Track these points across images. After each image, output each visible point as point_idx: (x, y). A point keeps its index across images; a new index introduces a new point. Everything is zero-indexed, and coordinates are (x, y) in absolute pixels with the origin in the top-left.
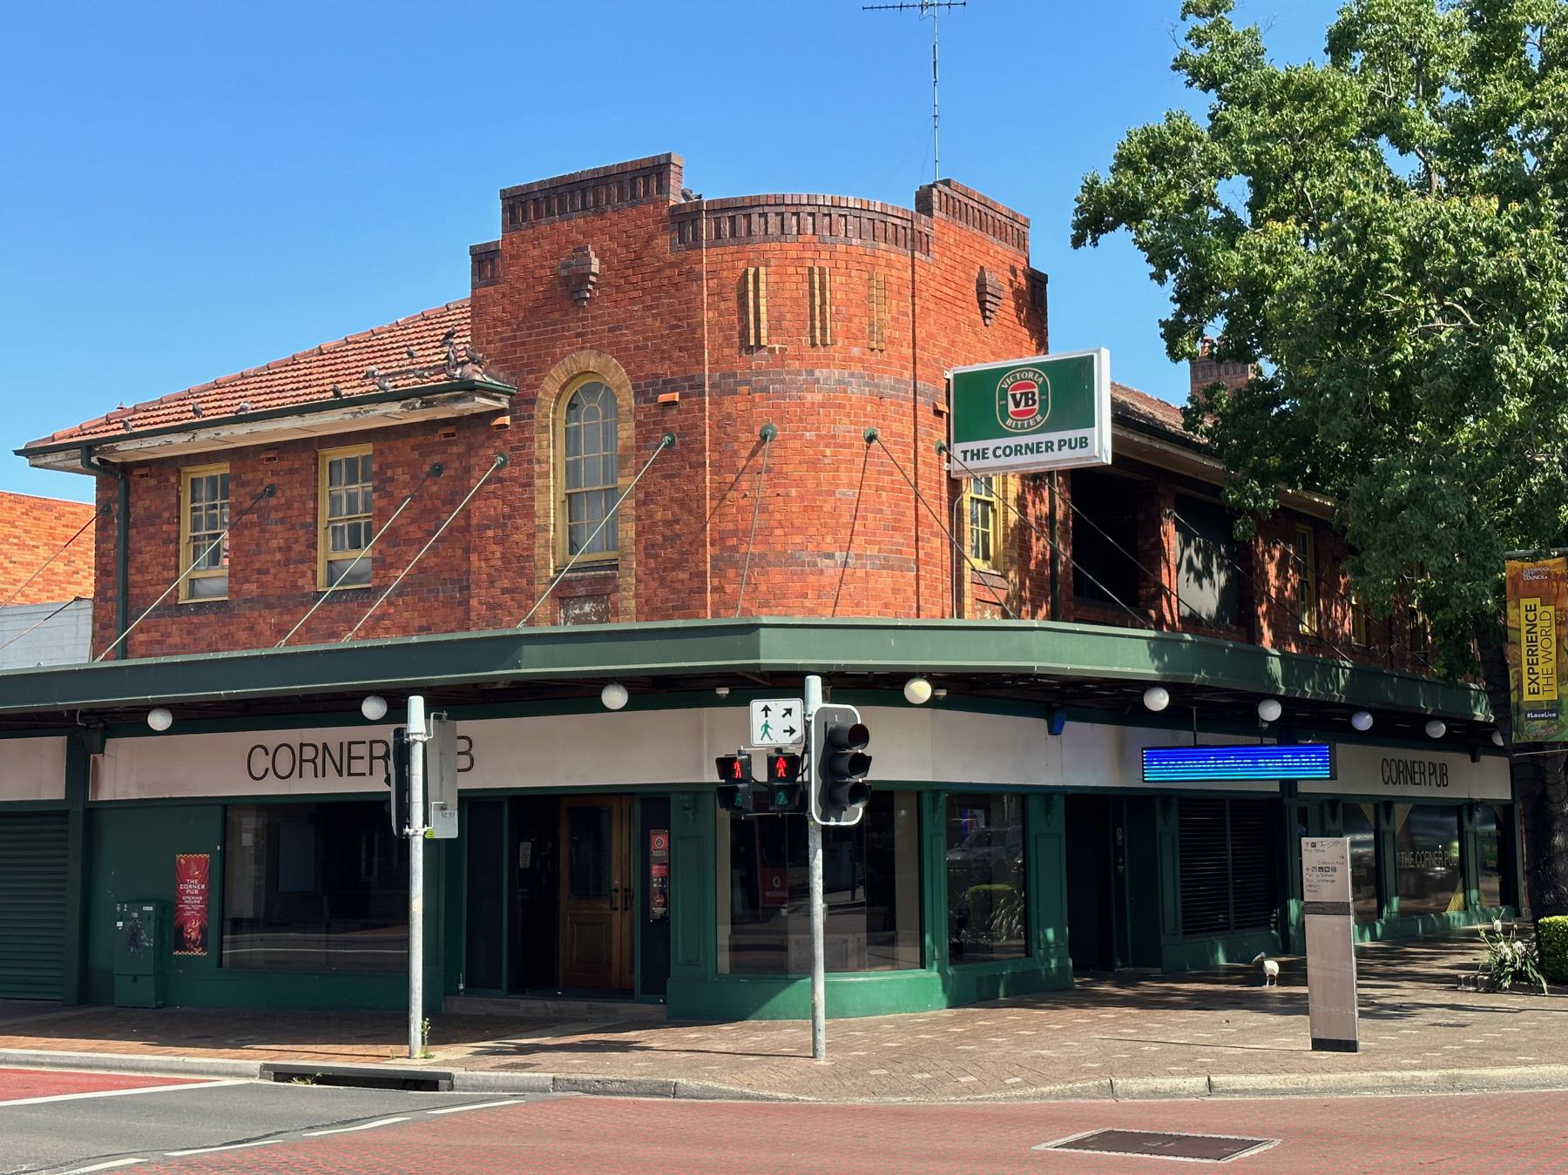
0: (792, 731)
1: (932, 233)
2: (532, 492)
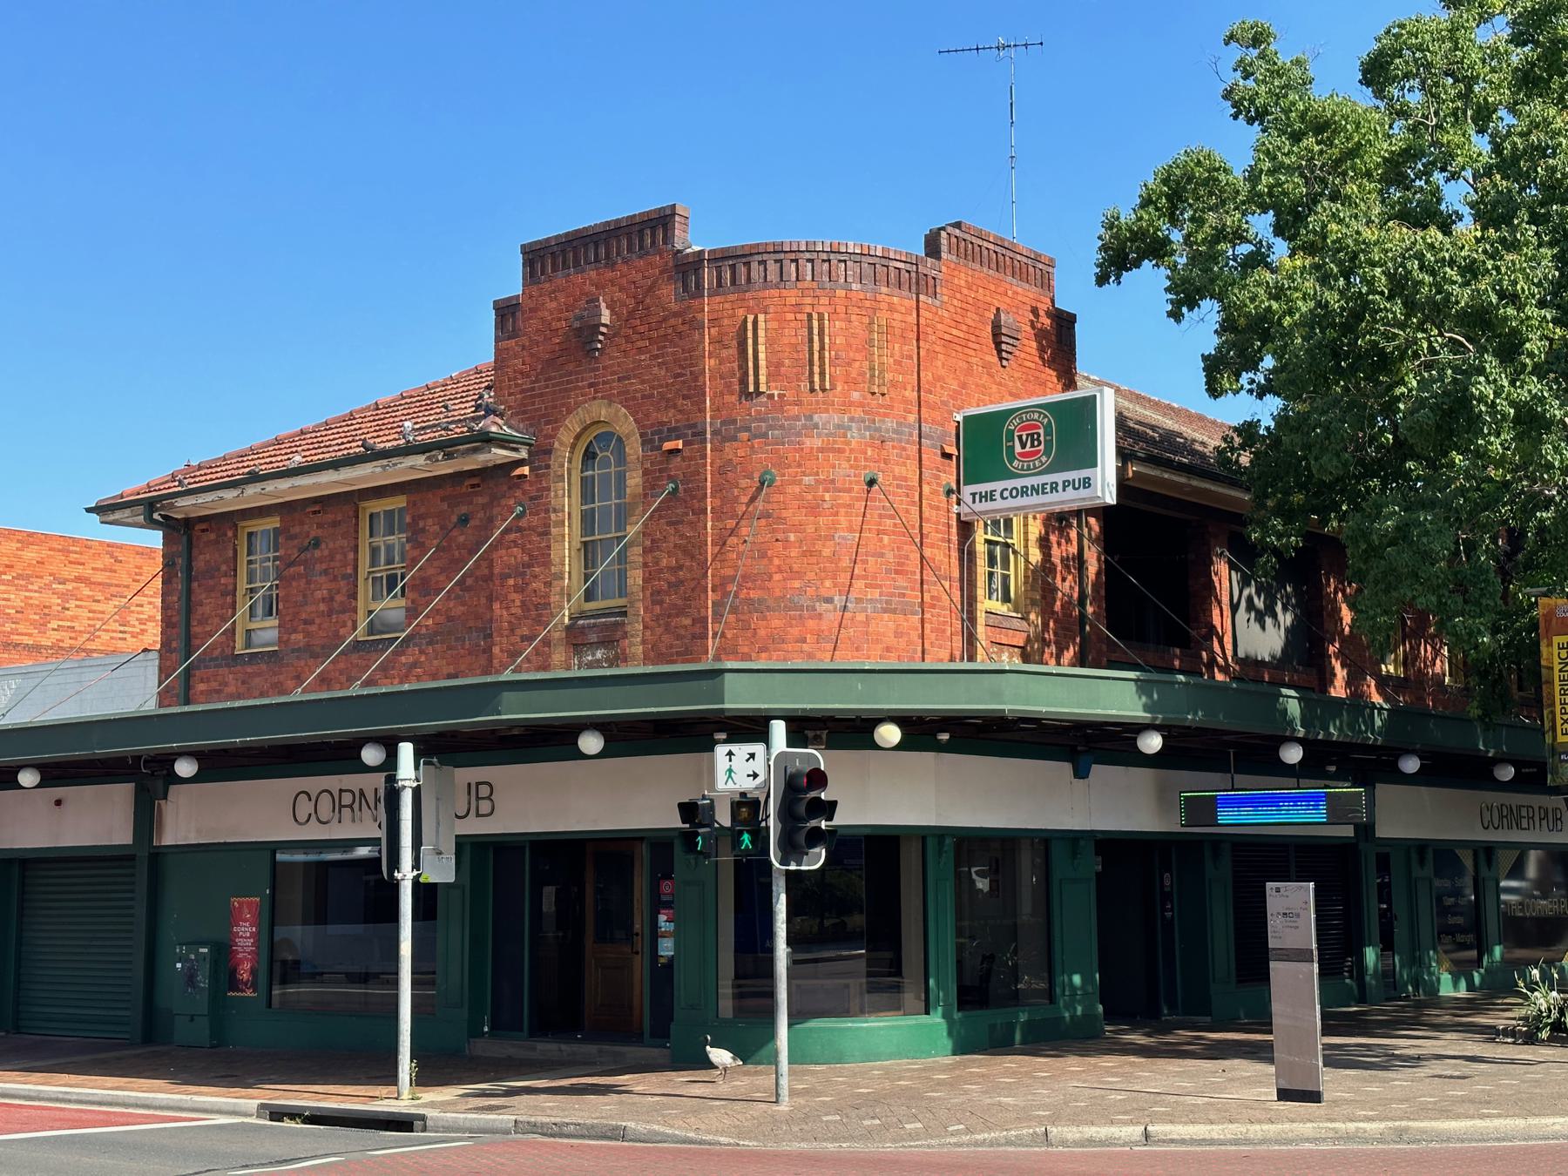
0: (755, 776)
1: (940, 276)
2: (549, 540)
